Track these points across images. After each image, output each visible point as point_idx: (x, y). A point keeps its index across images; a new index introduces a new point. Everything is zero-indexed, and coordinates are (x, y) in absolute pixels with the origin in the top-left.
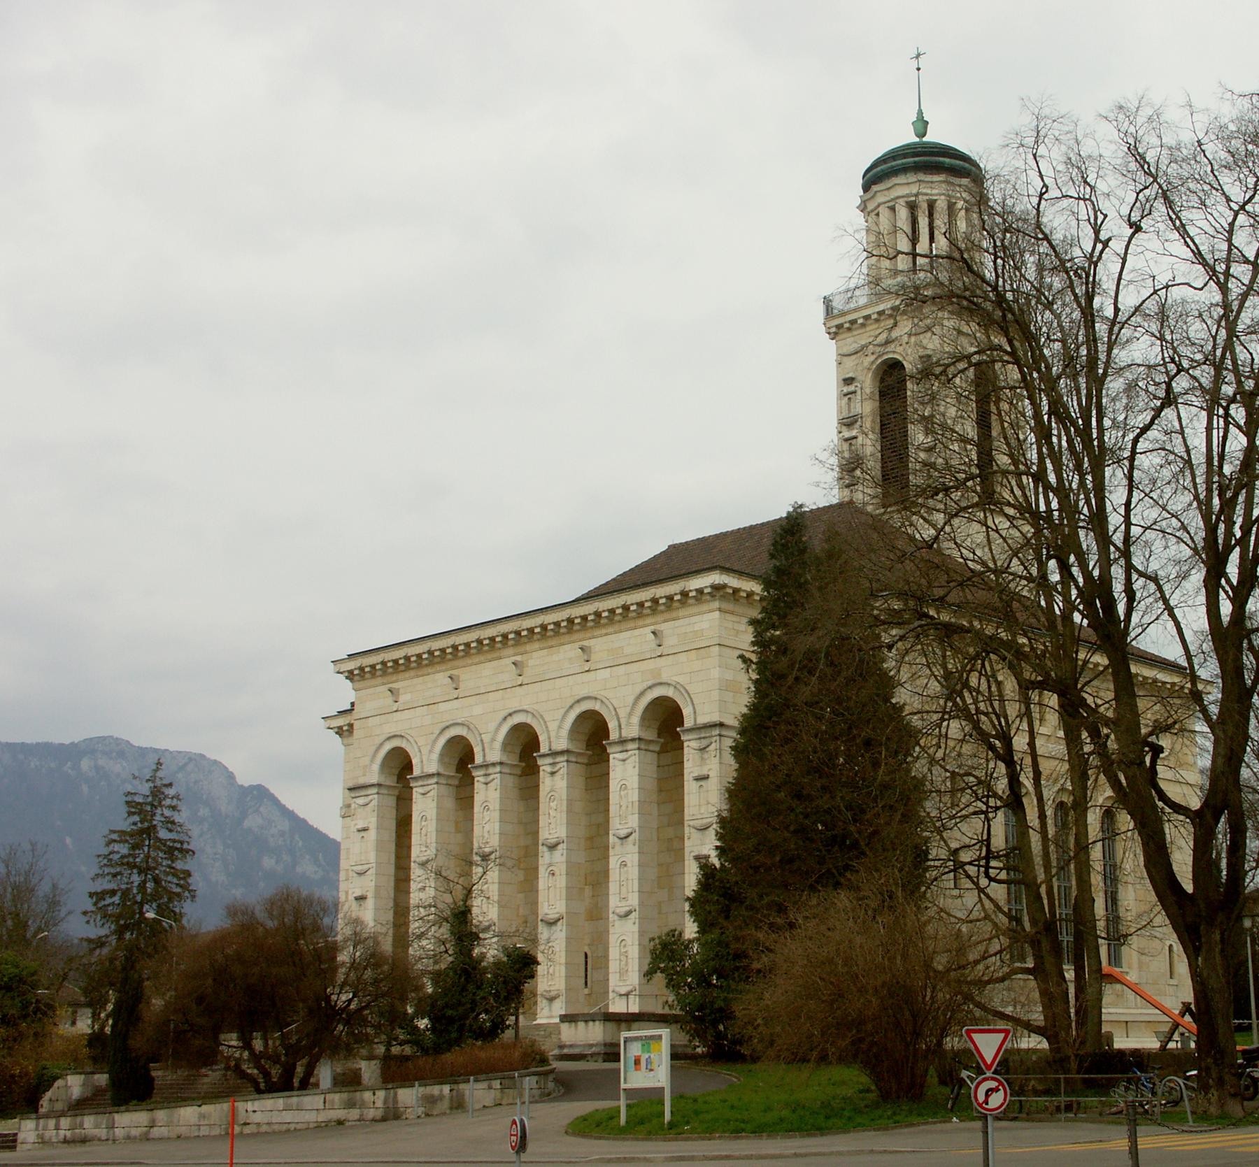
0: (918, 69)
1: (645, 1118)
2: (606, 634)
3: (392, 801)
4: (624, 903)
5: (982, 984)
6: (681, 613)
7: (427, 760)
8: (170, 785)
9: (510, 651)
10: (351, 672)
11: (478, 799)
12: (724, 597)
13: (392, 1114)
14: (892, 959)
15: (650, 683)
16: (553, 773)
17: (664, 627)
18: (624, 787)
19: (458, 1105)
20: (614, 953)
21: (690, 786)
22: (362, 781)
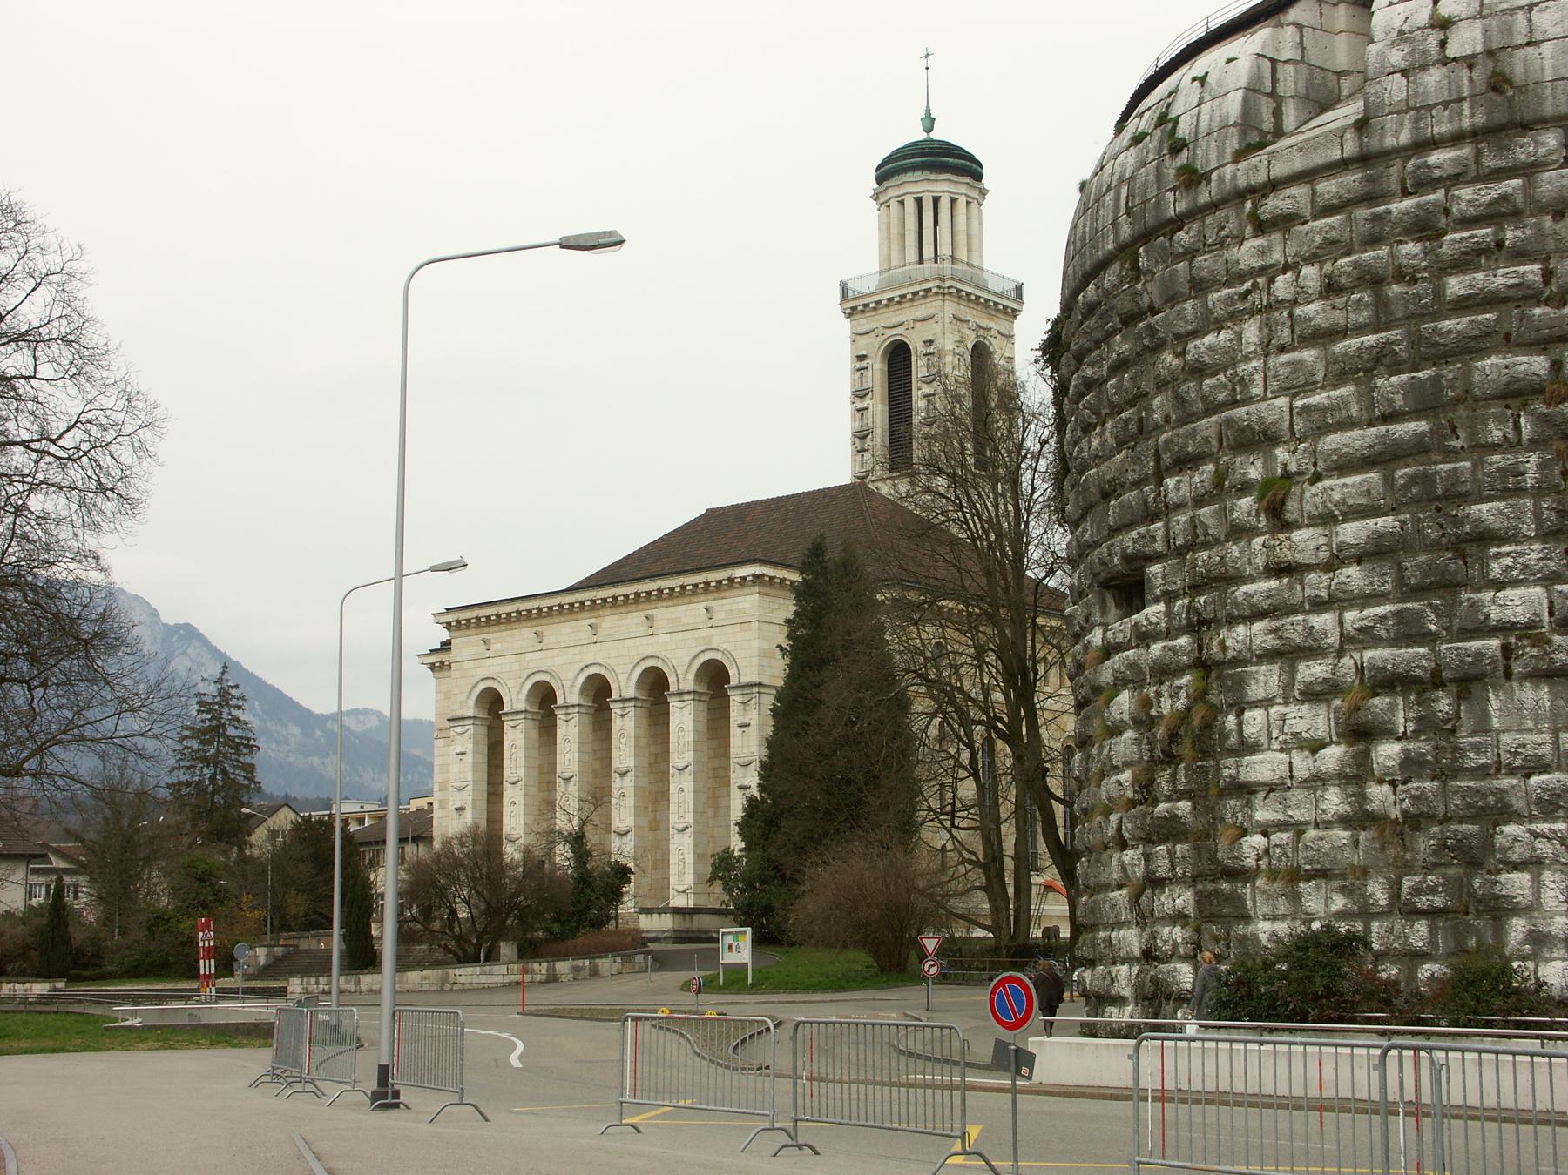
1: (735, 981)
3: (483, 730)
5: (947, 896)
6: (728, 594)
7: (516, 698)
8: (237, 686)
9: (586, 615)
10: (449, 624)
11: (560, 732)
12: (762, 584)
13: (552, 978)
14: (888, 887)
17: (713, 604)
18: (681, 729)
19: (595, 973)
20: (673, 859)
21: (735, 731)
22: (459, 714)
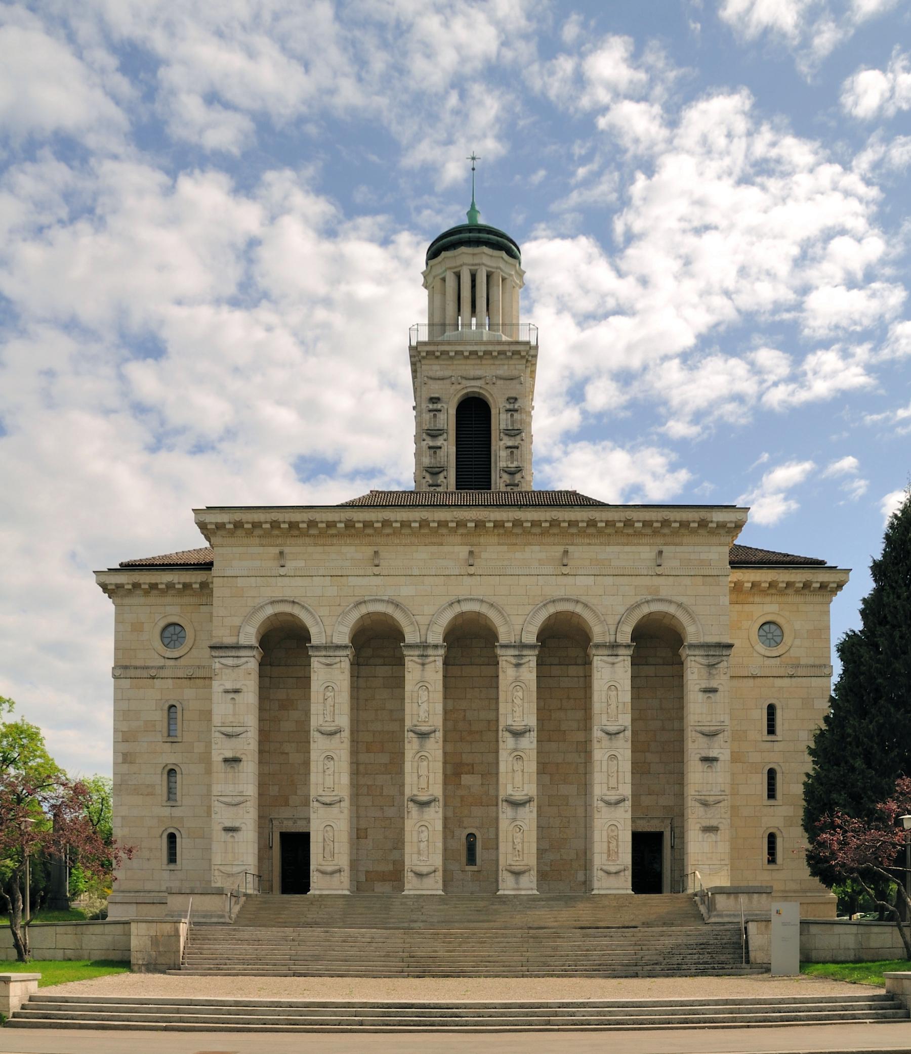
0: (473, 169)
2: (589, 544)
4: (613, 792)
15: (649, 598)
16: (518, 665)
